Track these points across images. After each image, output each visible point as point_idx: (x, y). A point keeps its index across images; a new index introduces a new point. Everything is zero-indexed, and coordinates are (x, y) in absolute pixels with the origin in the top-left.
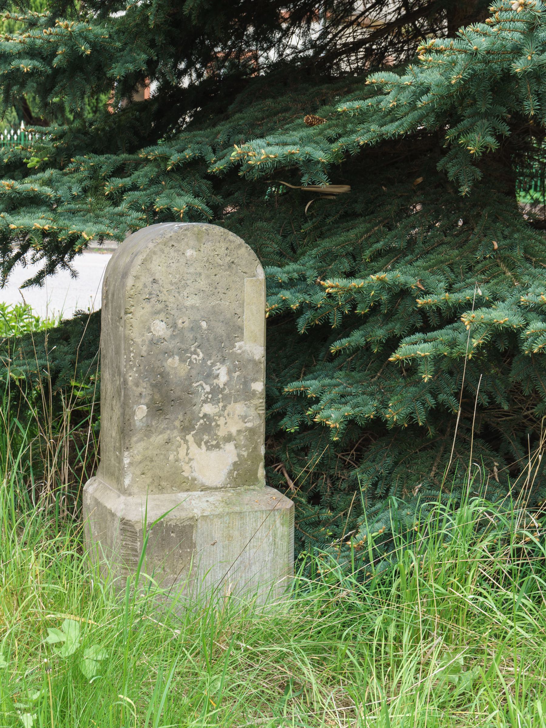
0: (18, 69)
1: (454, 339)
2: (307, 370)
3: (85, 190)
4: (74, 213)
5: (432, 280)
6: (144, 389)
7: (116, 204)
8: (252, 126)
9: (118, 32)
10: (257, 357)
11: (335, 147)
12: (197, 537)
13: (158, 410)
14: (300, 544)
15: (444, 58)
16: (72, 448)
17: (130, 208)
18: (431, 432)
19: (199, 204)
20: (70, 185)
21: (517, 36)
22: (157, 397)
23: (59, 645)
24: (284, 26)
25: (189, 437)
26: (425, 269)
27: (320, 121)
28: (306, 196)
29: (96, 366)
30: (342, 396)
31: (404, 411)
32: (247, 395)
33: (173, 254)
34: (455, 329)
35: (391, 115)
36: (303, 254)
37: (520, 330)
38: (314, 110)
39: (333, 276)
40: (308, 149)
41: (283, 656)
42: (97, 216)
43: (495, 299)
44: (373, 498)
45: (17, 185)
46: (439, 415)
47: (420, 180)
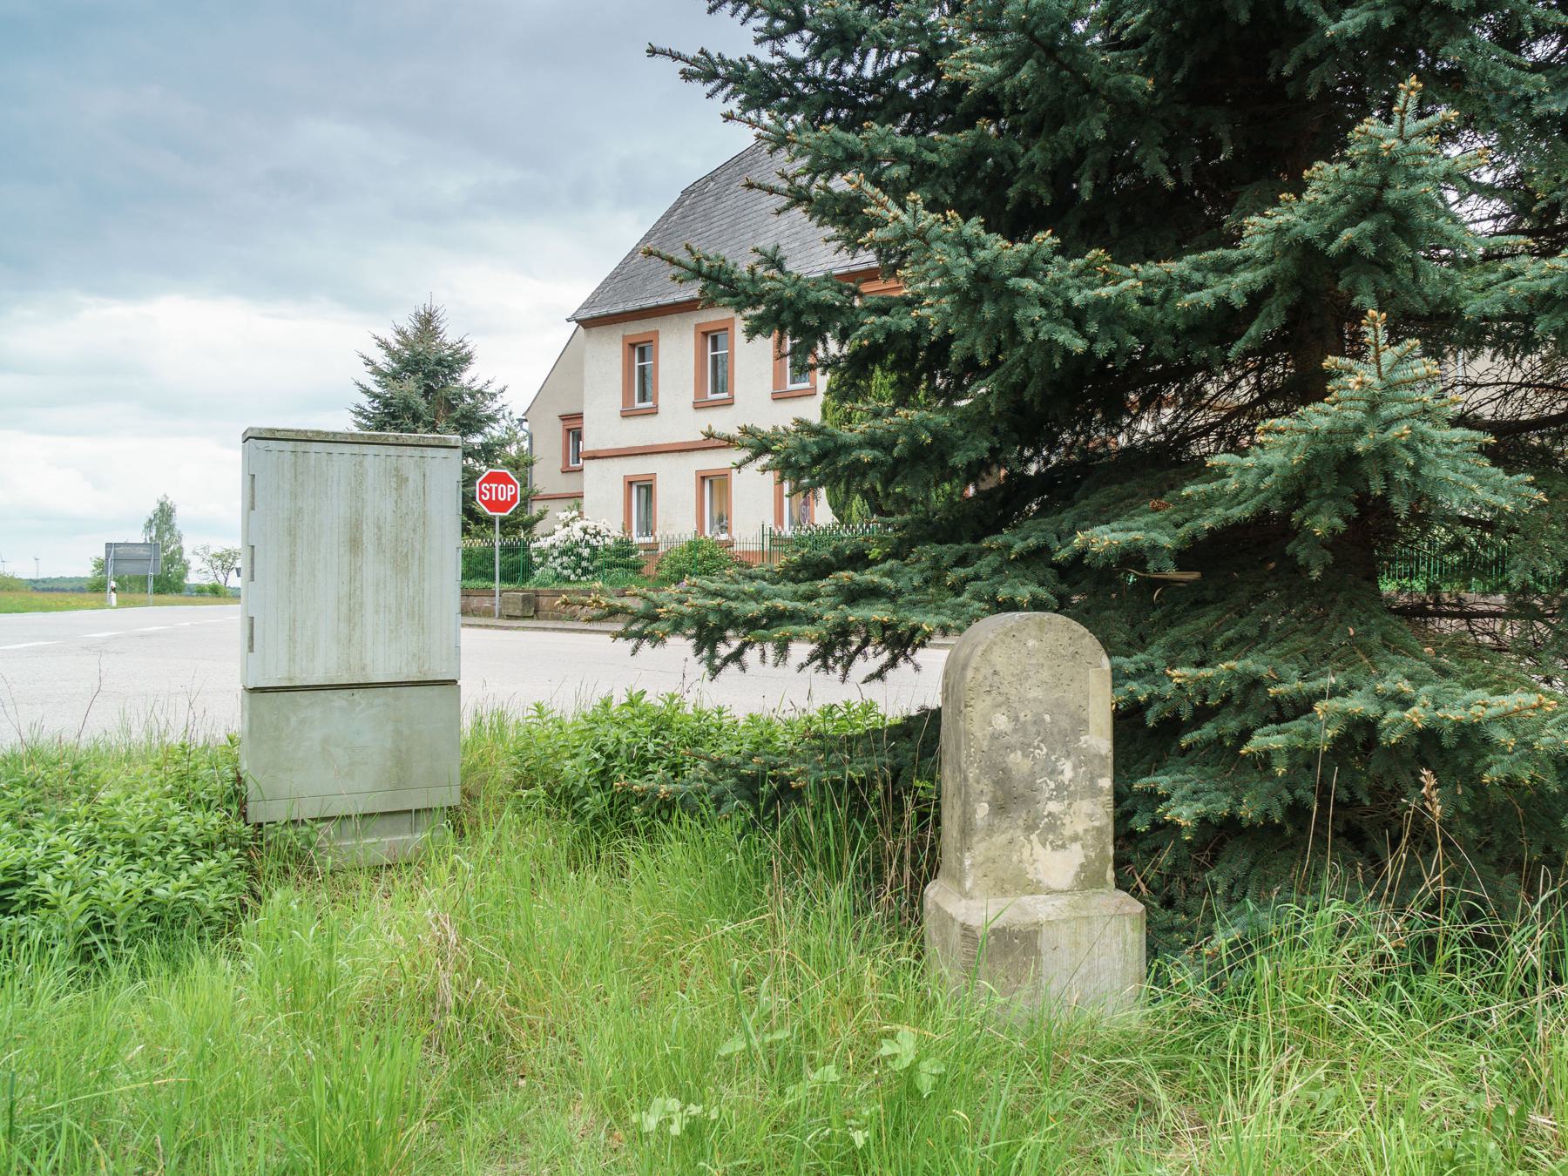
0: (859, 460)
1: (1309, 730)
2: (1157, 766)
3: (926, 581)
4: (914, 604)
5: (1284, 668)
6: (986, 785)
7: (958, 595)
8: (1098, 512)
9: (961, 420)
10: (1103, 752)
11: (1181, 532)
12: (1043, 943)
13: (1000, 808)
14: (1152, 951)
15: (1285, 439)
16: (914, 851)
17: (972, 598)
18: (1289, 830)
19: (1043, 593)
20: (912, 576)
21: (1359, 414)
22: (999, 793)
23: (894, 1057)
24: (1134, 412)
25: (1033, 837)
26: (1278, 657)
27: (1167, 506)
28: (1154, 584)
29: (938, 764)
30: (1195, 793)
31: (1259, 807)
32: (1095, 792)
33: (1014, 644)
34: (1310, 720)
35: (1235, 498)
36: (1151, 643)
37: (1378, 720)
38: (1162, 495)
39: (1182, 665)
40: (1153, 535)
41: (1131, 1070)
42: (939, 607)
43: (1351, 687)
44: (1230, 901)
45: (857, 577)
46: (1297, 811)
47: (1272, 565)
